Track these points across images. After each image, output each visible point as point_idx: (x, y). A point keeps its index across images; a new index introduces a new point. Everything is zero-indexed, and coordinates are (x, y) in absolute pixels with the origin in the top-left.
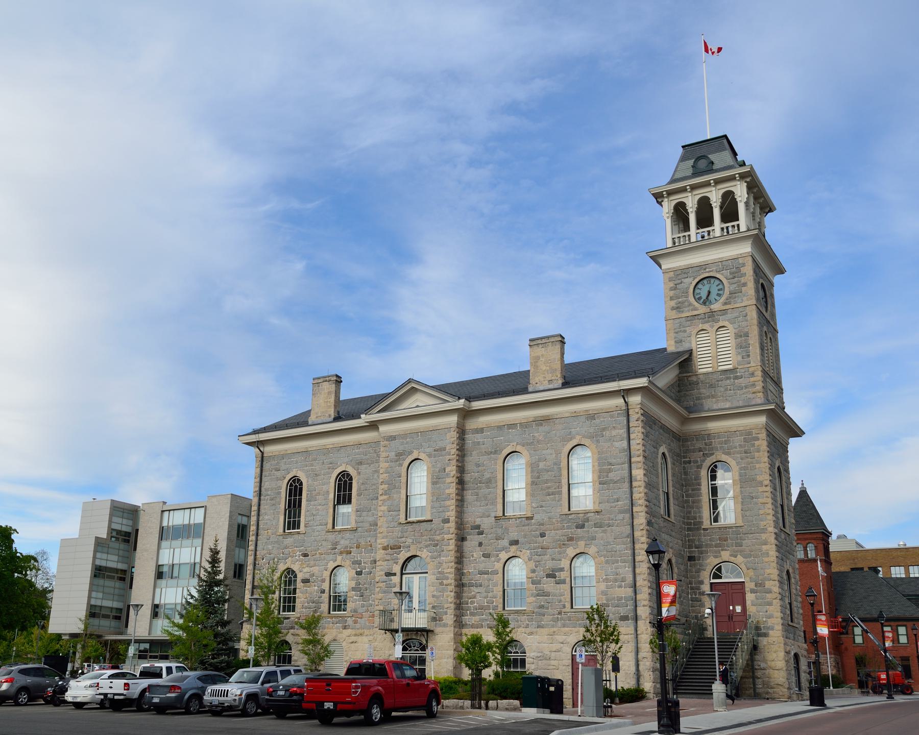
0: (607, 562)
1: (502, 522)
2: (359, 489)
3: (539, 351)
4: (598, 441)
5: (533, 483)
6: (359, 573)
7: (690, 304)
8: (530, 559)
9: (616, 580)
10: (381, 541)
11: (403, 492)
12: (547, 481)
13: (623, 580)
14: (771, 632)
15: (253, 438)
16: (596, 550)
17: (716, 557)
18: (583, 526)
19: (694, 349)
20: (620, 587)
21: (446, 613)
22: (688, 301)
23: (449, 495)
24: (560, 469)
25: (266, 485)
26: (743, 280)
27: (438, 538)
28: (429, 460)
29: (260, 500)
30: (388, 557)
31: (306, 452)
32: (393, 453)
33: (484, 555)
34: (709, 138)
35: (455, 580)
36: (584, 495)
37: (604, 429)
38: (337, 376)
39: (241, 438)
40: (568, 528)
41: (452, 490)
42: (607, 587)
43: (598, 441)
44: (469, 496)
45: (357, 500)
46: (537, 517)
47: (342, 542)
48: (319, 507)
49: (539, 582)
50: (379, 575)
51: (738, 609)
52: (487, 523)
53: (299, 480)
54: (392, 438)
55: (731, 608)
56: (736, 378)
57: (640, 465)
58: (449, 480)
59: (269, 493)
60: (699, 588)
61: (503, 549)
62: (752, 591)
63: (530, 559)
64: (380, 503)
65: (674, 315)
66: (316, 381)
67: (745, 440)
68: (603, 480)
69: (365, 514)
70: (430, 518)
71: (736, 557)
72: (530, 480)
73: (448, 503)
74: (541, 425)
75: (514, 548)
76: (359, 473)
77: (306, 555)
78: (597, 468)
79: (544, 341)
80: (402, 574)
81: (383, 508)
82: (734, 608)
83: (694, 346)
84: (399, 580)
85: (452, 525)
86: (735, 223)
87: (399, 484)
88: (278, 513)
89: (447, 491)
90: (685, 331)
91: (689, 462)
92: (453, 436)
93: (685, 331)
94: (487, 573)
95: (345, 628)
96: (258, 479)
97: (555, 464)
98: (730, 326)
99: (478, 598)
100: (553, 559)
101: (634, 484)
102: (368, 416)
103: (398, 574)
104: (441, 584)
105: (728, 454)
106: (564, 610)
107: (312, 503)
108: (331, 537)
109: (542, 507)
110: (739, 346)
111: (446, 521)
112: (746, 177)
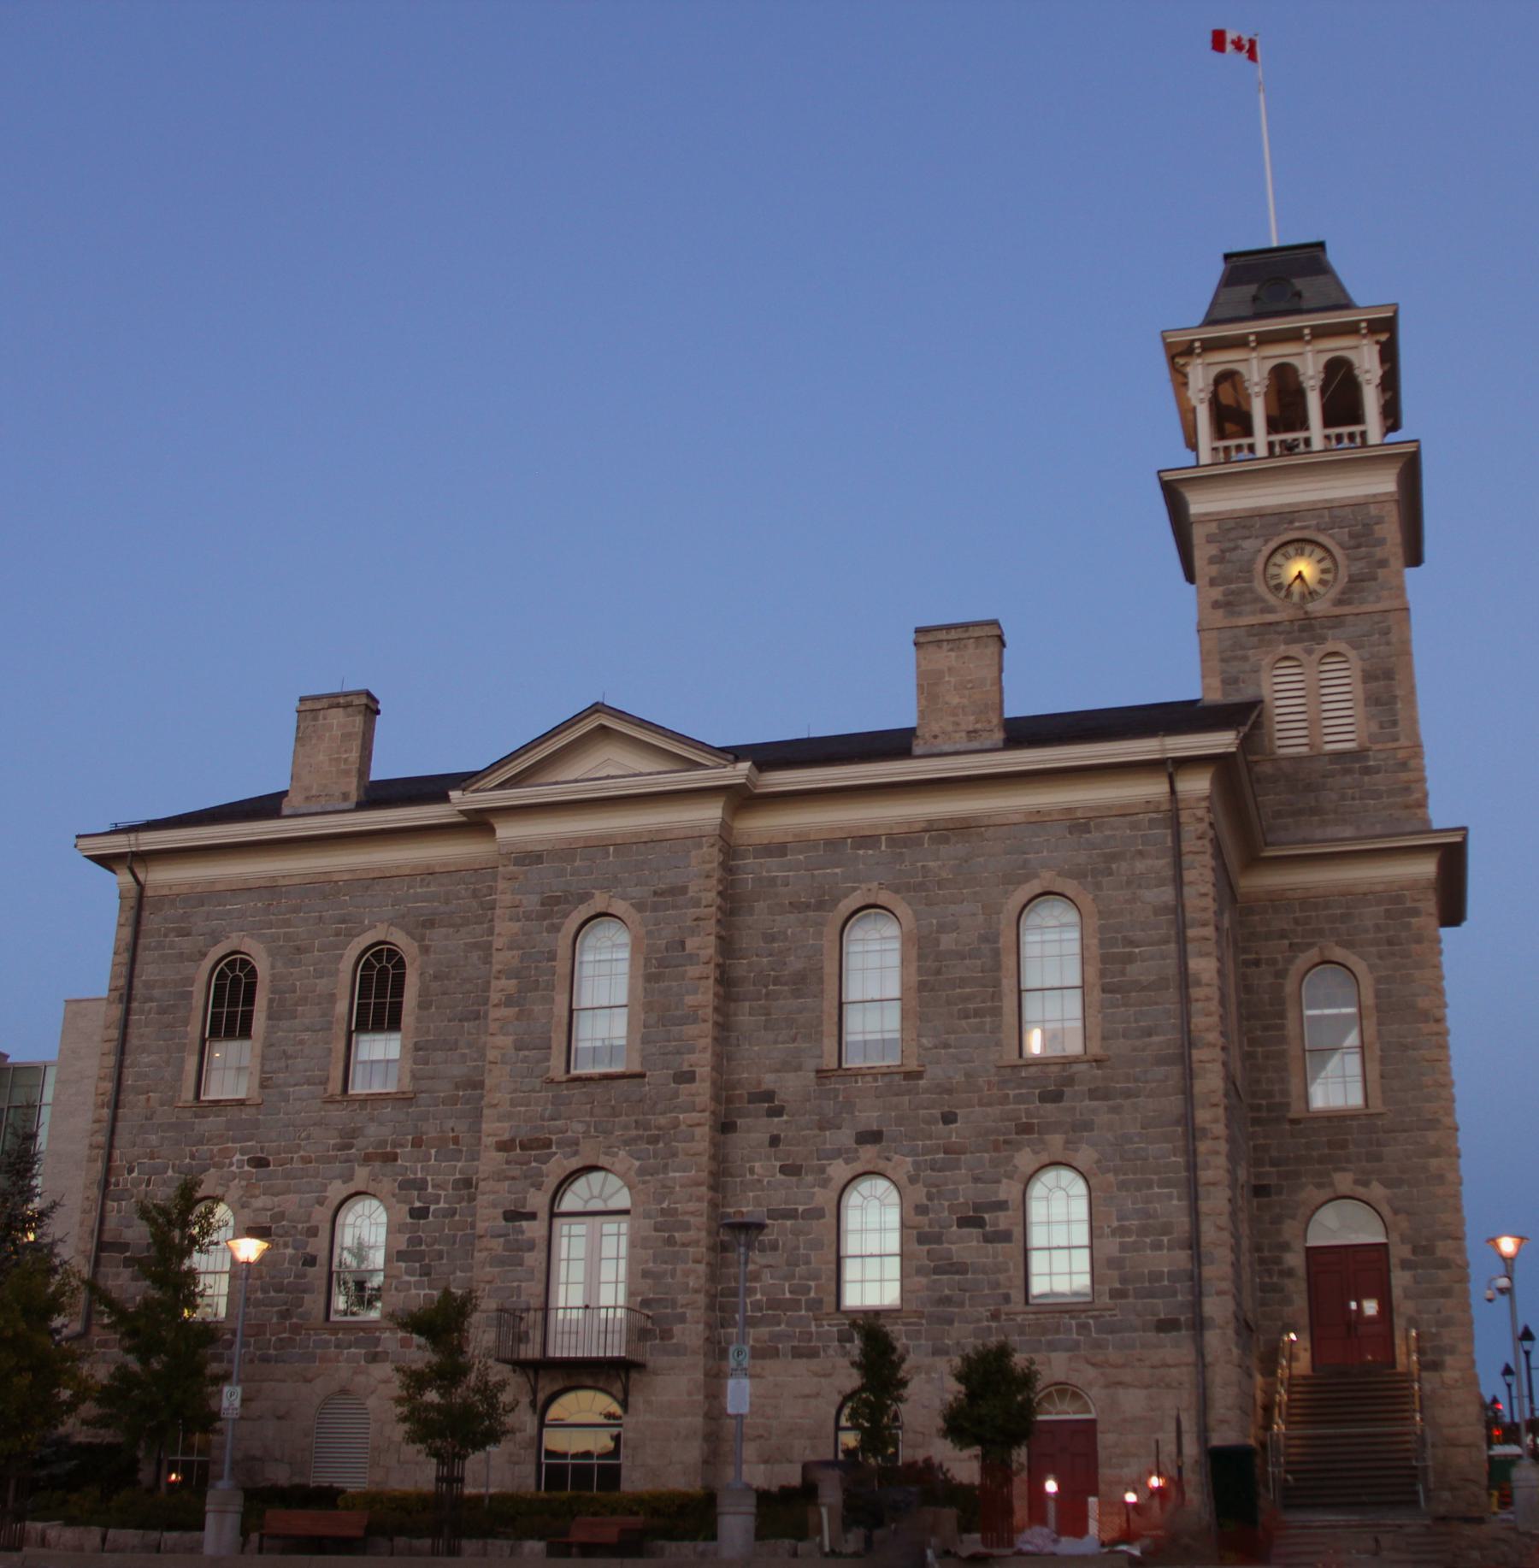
0: (1123, 1185)
1: (832, 1085)
2: (424, 992)
3: (943, 658)
4: (1098, 886)
5: (922, 986)
6: (419, 1214)
7: (1259, 599)
8: (913, 1180)
9: (1144, 1231)
10: (494, 1128)
11: (561, 999)
12: (963, 982)
13: (1166, 1229)
14: (1448, 1359)
15: (121, 844)
16: (1096, 1156)
17: (1319, 1186)
18: (1057, 1097)
19: (1267, 699)
20: (1157, 1246)
21: (682, 1319)
22: (1251, 590)
23: (696, 1008)
24: (996, 953)
25: (148, 971)
26: (1379, 553)
27: (662, 1121)
28: (637, 916)
29: (128, 1012)
30: (516, 1171)
31: (270, 890)
32: (535, 898)
33: (784, 1170)
34: (1275, 244)
35: (709, 1233)
36: (1050, 1027)
37: (1114, 857)
38: (368, 694)
39: (84, 843)
40: (1020, 1099)
41: (704, 996)
42: (1123, 1247)
43: (1098, 886)
44: (745, 1017)
45: (419, 1020)
46: (934, 1073)
47: (372, 1129)
48: (306, 1036)
49: (937, 1239)
50: (488, 1217)
51: (1371, 1307)
52: (790, 1086)
53: (245, 963)
54: (529, 857)
55: (1353, 1305)
56: (1367, 771)
57: (1211, 947)
58: (693, 971)
59: (156, 992)
60: (1278, 1261)
61: (838, 1153)
62: (1406, 1265)
63: (913, 1180)
64: (493, 1026)
65: (1218, 618)
66: (309, 705)
67: (1388, 914)
68: (1109, 977)
69: (439, 1056)
70: (636, 1068)
71: (1366, 1184)
72: (914, 979)
73: (691, 1030)
74: (946, 840)
75: (868, 1152)
76: (425, 950)
77: (260, 1163)
78: (1095, 951)
79: (953, 635)
80: (553, 1215)
81: (500, 1040)
82: (1359, 1306)
83: (1266, 693)
84: (544, 1232)
85: (702, 1090)
86: (1356, 429)
87: (547, 981)
88: (182, 1048)
89: (690, 1000)
90: (1245, 658)
91: (1257, 963)
92: (707, 858)
93: (1245, 658)
94: (791, 1214)
95: (374, 1358)
96: (125, 958)
97: (984, 939)
98: (1352, 654)
99: (767, 1279)
100: (976, 1180)
101: (1195, 992)
102: (469, 796)
103: (543, 1215)
104: (670, 1241)
105: (1348, 945)
106: (1005, 1308)
107: (284, 1024)
108: (338, 1114)
109: (946, 1046)
110: (1373, 700)
111: (687, 1077)
112: (1381, 331)
